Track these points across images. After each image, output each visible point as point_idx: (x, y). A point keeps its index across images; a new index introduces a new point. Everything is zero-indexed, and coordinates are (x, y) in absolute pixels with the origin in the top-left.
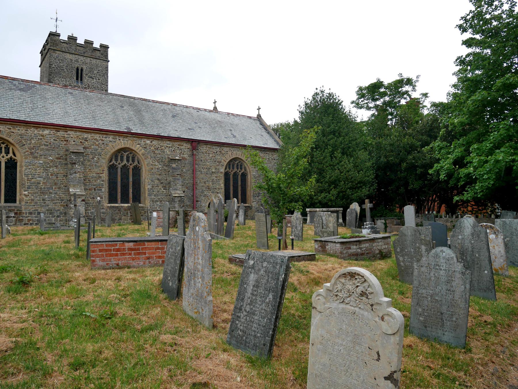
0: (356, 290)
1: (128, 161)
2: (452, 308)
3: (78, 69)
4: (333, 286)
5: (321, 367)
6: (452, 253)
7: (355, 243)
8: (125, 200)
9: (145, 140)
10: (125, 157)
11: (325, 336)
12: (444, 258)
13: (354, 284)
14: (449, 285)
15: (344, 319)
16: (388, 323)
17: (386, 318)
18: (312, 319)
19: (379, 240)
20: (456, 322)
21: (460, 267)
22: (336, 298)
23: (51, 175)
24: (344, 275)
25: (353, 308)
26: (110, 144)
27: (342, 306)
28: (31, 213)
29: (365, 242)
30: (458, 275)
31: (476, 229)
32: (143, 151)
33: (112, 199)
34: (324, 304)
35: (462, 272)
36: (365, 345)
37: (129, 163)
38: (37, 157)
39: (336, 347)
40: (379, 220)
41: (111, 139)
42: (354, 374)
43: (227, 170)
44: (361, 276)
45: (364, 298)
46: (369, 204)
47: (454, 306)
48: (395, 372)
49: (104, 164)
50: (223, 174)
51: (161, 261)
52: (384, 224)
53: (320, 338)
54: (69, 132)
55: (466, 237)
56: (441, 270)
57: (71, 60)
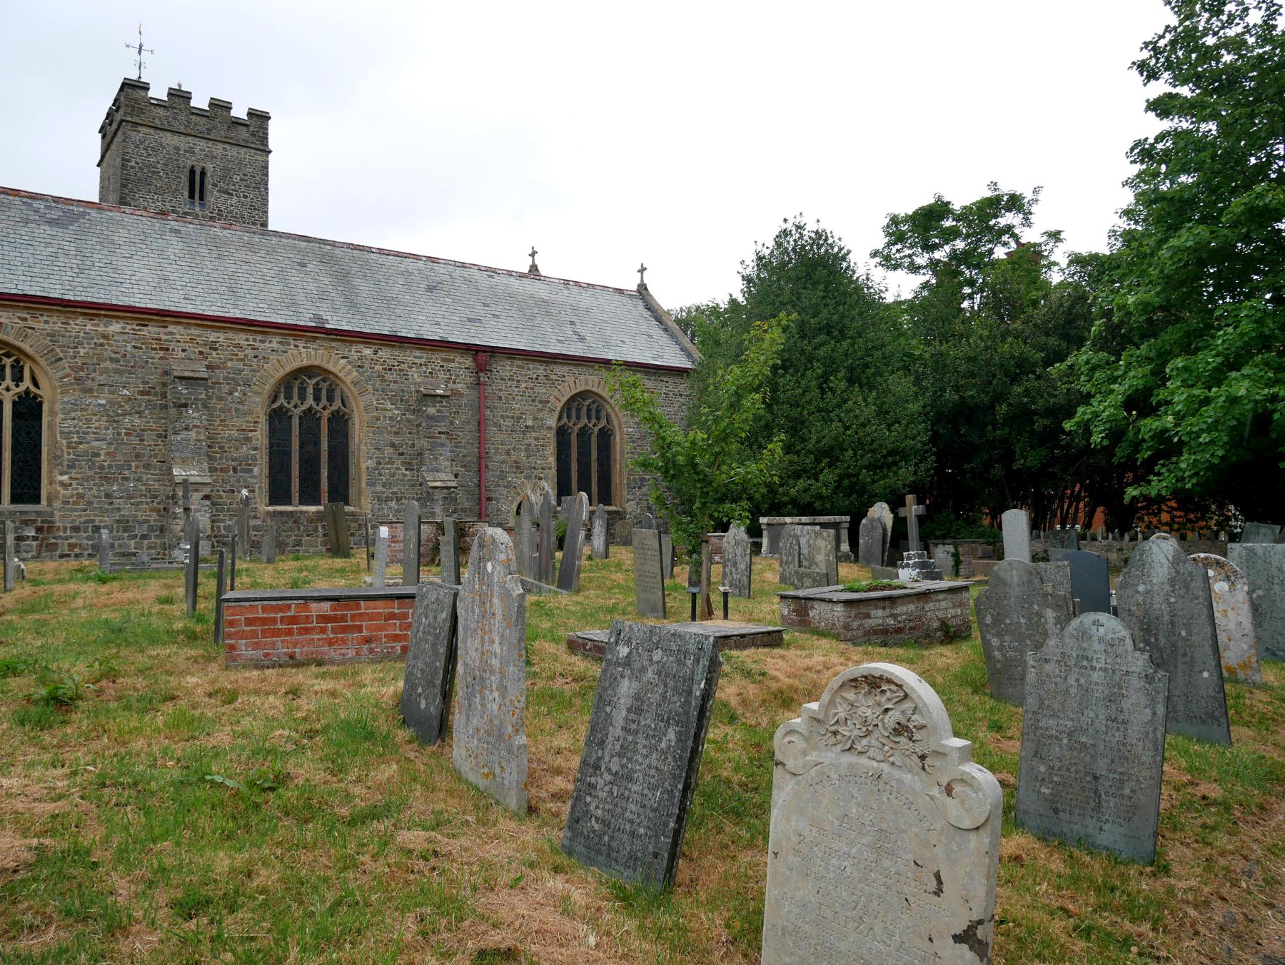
0: (882, 720)
1: (317, 398)
2: (1122, 765)
3: (192, 171)
4: (827, 709)
5: (796, 911)
6: (1120, 628)
7: (881, 604)
8: (310, 496)
9: (361, 347)
10: (310, 391)
11: (806, 833)
12: (1101, 640)
13: (879, 705)
14: (1114, 707)
15: (855, 792)
16: (963, 802)
17: (957, 788)
18: (774, 792)
19: (941, 596)
20: (1130, 798)
21: (1140, 663)
22: (833, 740)
23: (127, 434)
24: (854, 683)
25: (875, 764)
26: (274, 357)
27: (849, 758)
28: (76, 529)
29: (906, 600)
30: (1136, 683)
31: (1181, 568)
32: (355, 374)
33: (278, 493)
34: (805, 754)
35: (1146, 676)
36: (904, 857)
37: (321, 405)
38: (91, 390)
39: (834, 861)
40: (940, 546)
41: (275, 345)
42: (878, 928)
43: (562, 423)
44: (897, 685)
45: (903, 740)
46: (914, 507)
47: (1127, 759)
48: (980, 922)
49: (258, 406)
50: (553, 432)
51: (399, 649)
52: (953, 555)
53: (795, 839)
54: (171, 328)
55: (1156, 588)
56: (1093, 669)
57: (177, 149)
